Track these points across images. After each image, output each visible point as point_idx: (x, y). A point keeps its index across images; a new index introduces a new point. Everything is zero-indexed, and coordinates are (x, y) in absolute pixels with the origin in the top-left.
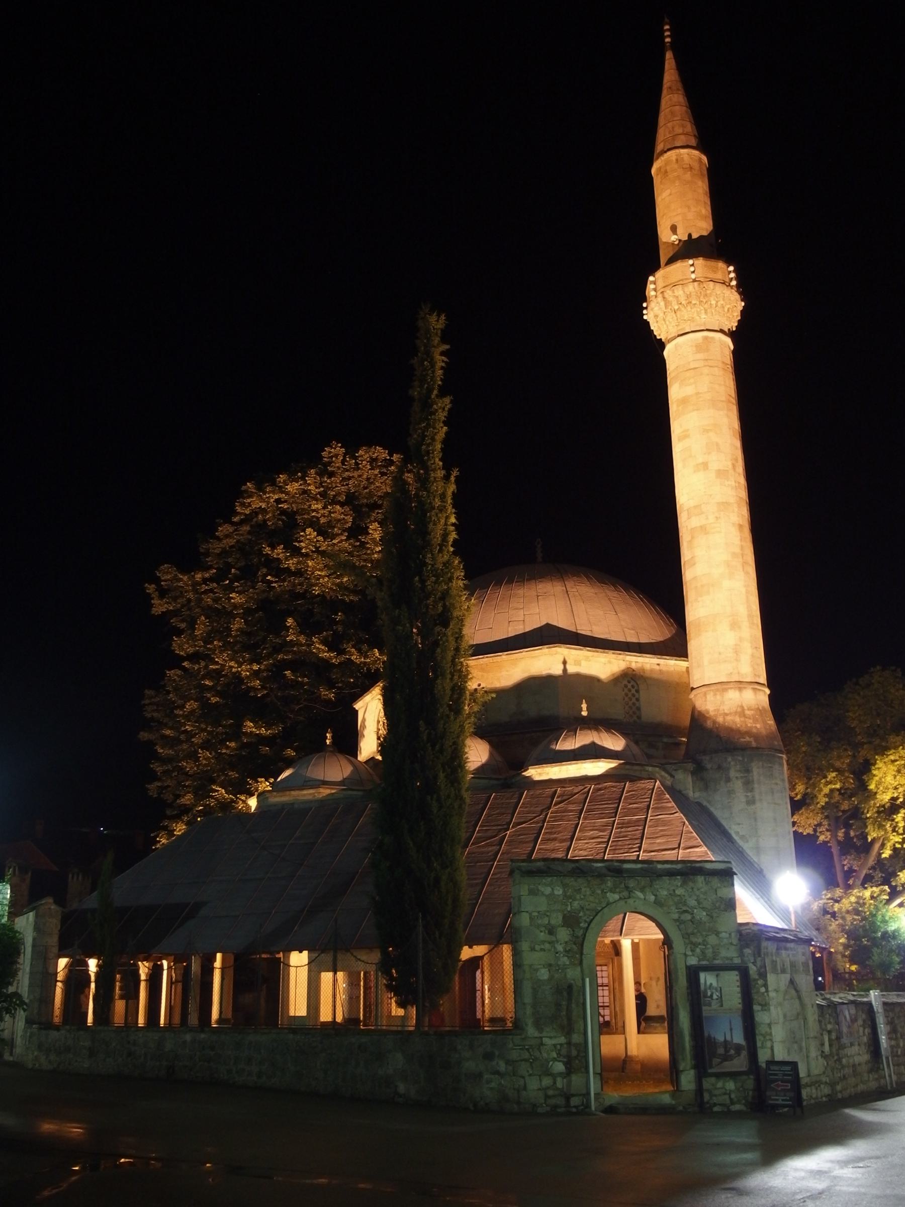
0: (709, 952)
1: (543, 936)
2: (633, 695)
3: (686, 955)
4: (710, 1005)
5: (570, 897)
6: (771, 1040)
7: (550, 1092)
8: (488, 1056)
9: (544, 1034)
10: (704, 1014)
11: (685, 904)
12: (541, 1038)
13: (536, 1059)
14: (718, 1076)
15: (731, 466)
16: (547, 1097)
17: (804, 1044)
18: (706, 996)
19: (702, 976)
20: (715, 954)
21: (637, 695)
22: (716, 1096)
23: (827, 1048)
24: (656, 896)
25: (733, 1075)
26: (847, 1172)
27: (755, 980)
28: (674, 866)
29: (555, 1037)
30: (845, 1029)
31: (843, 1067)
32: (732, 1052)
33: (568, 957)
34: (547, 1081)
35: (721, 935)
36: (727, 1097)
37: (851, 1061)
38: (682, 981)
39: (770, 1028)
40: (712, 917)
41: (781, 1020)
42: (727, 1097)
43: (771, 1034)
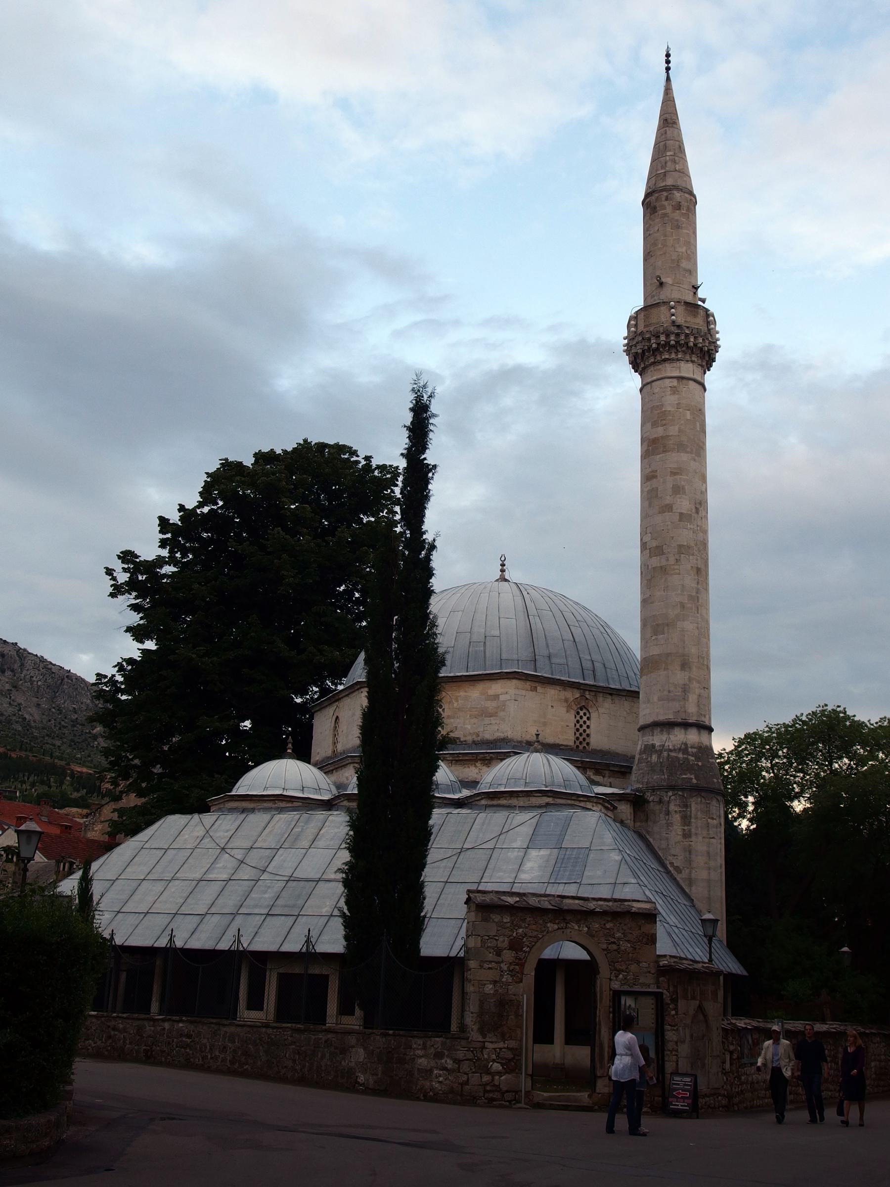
1: (491, 956)
3: (610, 979)
5: (516, 925)
7: (488, 1088)
8: (438, 1055)
9: (487, 1039)
11: (613, 936)
12: (484, 1042)
13: (479, 1059)
15: (694, 511)
16: (485, 1091)
21: (588, 723)
23: (727, 1066)
24: (589, 928)
27: (669, 1004)
29: (496, 1042)
30: (746, 1051)
33: (512, 976)
34: (486, 1078)
37: (750, 1079)
40: (635, 949)
41: (688, 1039)
43: (677, 1051)
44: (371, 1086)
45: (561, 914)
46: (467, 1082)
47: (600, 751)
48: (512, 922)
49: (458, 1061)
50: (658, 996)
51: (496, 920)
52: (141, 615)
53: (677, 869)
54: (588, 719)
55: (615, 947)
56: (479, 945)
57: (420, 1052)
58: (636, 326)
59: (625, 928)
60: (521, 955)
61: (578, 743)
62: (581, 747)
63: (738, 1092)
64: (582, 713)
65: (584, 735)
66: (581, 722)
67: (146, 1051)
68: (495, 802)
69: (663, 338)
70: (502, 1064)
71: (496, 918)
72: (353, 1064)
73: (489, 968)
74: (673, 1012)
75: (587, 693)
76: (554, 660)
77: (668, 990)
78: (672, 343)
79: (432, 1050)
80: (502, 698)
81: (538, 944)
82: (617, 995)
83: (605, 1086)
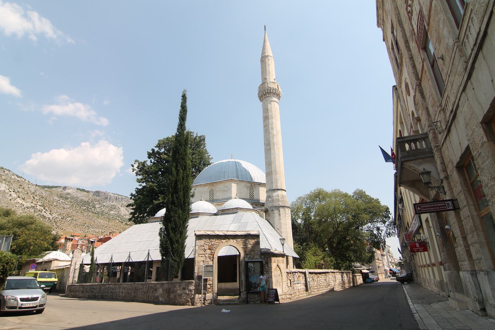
2: (252, 195)
4: (251, 272)
6: (269, 282)
8: (184, 289)
10: (249, 275)
14: (253, 293)
18: (250, 269)
19: (249, 264)
20: (253, 257)
22: (251, 299)
26: (368, 280)
30: (296, 279)
35: (255, 252)
36: (255, 299)
37: (298, 288)
39: (269, 279)
43: (269, 281)
44: (163, 302)
50: (261, 262)
52: (296, 256)
53: (278, 229)
54: (253, 191)
61: (250, 198)
62: (251, 199)
63: (294, 293)
64: (251, 190)
66: (251, 192)
67: (101, 295)
68: (224, 213)
72: (158, 295)
73: (201, 256)
80: (229, 187)
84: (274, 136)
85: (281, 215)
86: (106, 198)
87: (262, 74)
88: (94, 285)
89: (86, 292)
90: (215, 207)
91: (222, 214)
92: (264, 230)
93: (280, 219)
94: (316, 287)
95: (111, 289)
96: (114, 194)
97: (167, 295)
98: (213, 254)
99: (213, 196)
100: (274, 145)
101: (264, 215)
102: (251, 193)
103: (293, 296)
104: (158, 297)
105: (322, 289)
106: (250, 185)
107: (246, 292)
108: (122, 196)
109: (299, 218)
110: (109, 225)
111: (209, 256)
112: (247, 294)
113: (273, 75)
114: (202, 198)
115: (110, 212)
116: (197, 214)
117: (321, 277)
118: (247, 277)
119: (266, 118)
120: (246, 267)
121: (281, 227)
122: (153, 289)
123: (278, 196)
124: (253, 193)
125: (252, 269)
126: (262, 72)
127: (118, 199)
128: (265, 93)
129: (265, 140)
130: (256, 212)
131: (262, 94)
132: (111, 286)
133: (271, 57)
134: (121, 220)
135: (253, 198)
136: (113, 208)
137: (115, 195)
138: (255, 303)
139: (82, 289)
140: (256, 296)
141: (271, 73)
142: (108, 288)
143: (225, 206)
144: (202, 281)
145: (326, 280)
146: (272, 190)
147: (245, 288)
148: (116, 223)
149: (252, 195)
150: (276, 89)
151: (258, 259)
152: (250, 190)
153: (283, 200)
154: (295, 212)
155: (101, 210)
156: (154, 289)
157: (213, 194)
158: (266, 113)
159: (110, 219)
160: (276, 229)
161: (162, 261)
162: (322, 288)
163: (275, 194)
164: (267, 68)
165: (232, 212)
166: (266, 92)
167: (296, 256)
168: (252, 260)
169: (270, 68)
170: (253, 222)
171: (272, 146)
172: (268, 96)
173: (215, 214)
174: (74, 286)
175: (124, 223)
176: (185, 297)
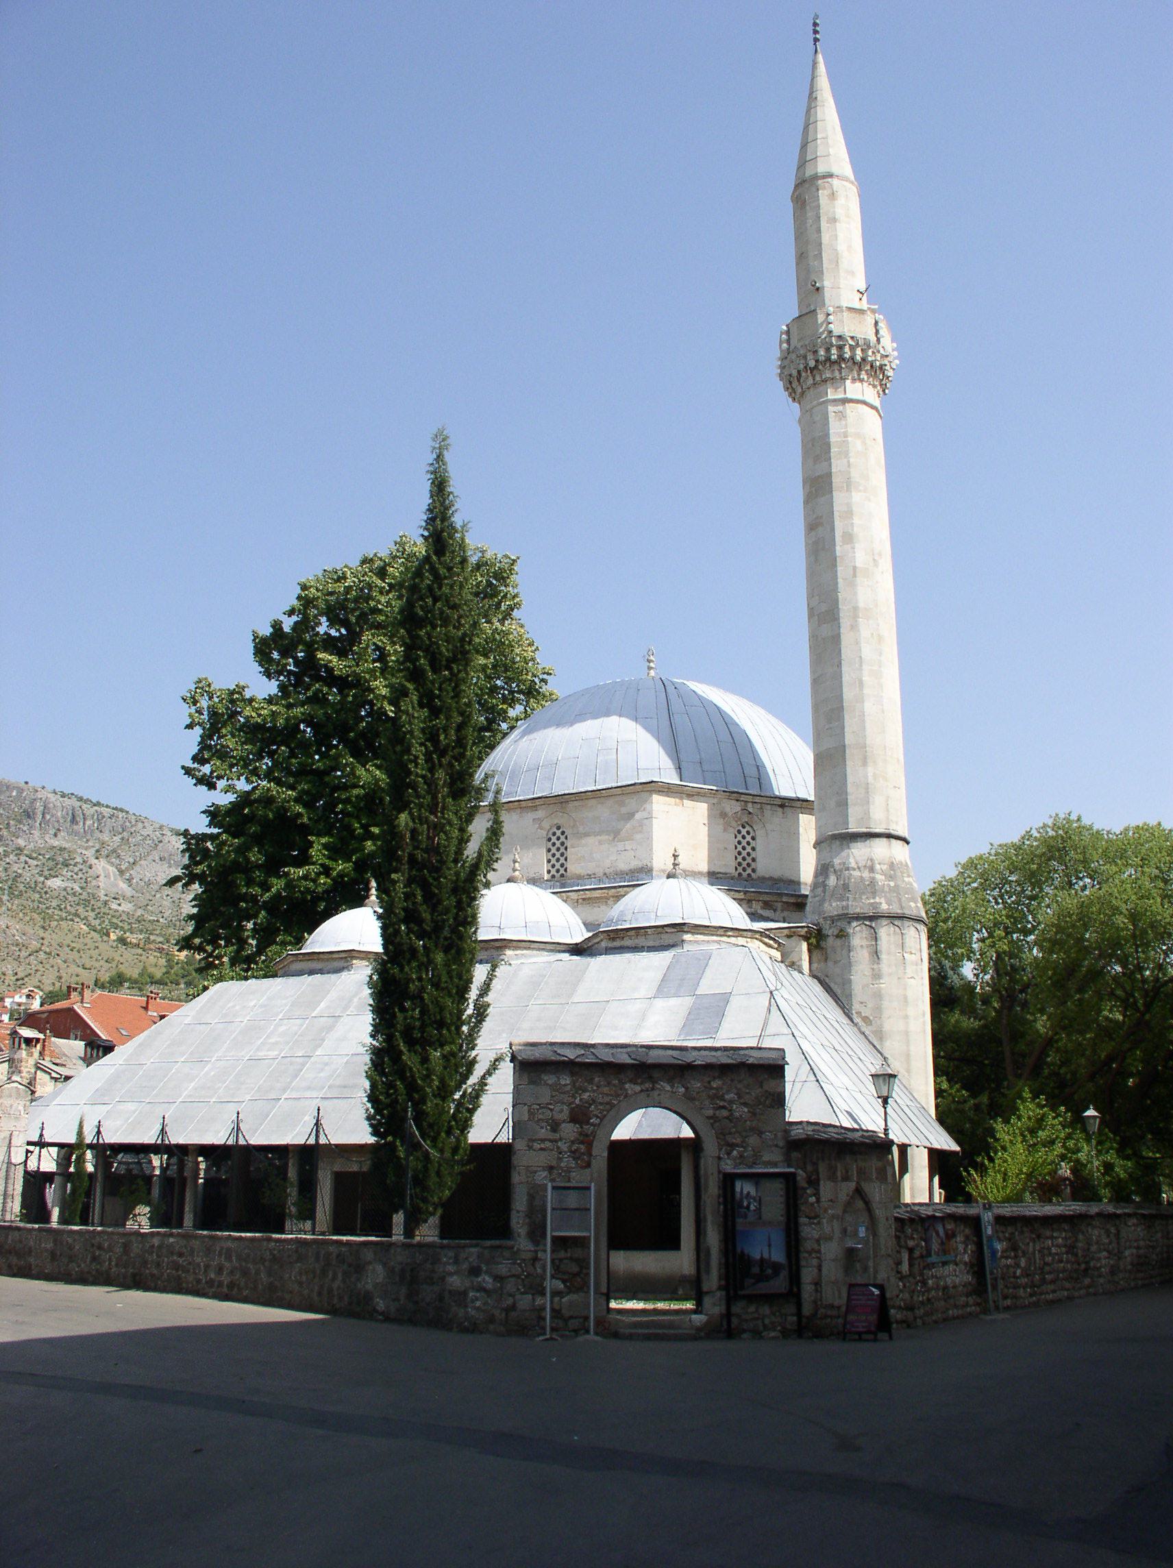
0: (748, 1153)
1: (544, 1133)
2: (748, 843)
3: (719, 1158)
4: (745, 1216)
8: (475, 1271)
10: (739, 1228)
12: (536, 1252)
14: (751, 1299)
17: (871, 1264)
18: (741, 1206)
21: (753, 843)
23: (905, 1268)
24: (687, 1089)
25: (768, 1298)
28: (713, 1053)
30: (935, 1246)
31: (929, 1290)
32: (770, 1271)
38: (712, 1189)
41: (837, 1234)
42: (759, 1322)
43: (819, 1251)
45: (646, 1073)
46: (514, 1307)
47: (771, 878)
48: (574, 1083)
49: (498, 1278)
50: (789, 1178)
51: (550, 1082)
52: (946, 1143)
53: (865, 1019)
55: (725, 1113)
56: (526, 1117)
57: (451, 1268)
58: (788, 342)
59: (739, 1086)
60: (588, 1129)
62: (745, 874)
63: (922, 1303)
64: (744, 832)
65: (749, 860)
66: (744, 843)
68: (617, 943)
69: (822, 352)
70: (564, 1281)
71: (550, 1079)
72: (369, 1287)
73: (542, 1149)
74: (813, 1199)
75: (750, 805)
76: (705, 767)
77: (804, 1169)
78: (834, 357)
79: (465, 1266)
81: (612, 1113)
82: (728, 1180)
83: (715, 1304)
84: (855, 575)
85: (883, 956)
86: (29, 815)
87: (797, 264)
88: (100, 1233)
89: (70, 1257)
90: (573, 908)
91: (608, 951)
92: (802, 1029)
93: (877, 976)
94: (1024, 1280)
95: (172, 1253)
96: (63, 796)
97: (404, 1291)
98: (587, 1140)
99: (562, 860)
100: (855, 617)
101: (805, 956)
102: (744, 848)
103: (920, 1312)
104: (368, 1297)
105: (1051, 1287)
106: (737, 807)
107: (724, 1293)
108: (98, 804)
109: (969, 959)
110: (46, 942)
111: (574, 1148)
112: (729, 1301)
113: (852, 273)
114: (514, 870)
115: (48, 883)
116: (497, 944)
117: (1052, 1238)
118: (730, 1236)
119: (819, 486)
120: (725, 1197)
121: (878, 1009)
122: (345, 1267)
123: (872, 869)
124: (753, 849)
125: (749, 1204)
126: (801, 257)
127: (80, 819)
128: (812, 364)
129: (810, 596)
130: (766, 944)
131: (802, 366)
132: (171, 1240)
133: (847, 180)
134: (98, 922)
135: (754, 871)
136: (58, 861)
137: (67, 802)
138: (757, 1334)
139: (50, 1246)
140: (766, 1310)
141: (844, 264)
142: (160, 1247)
143: (622, 913)
144: (545, 1245)
145: (1071, 1249)
146: (838, 839)
147: (720, 1279)
148: (75, 933)
149: (745, 858)
150: (868, 345)
151: (775, 1165)
152: (739, 832)
153: (892, 884)
154: (945, 942)
155: (6, 870)
156: (350, 1265)
157: (562, 850)
158: (817, 459)
159: (51, 917)
160: (857, 1020)
161: (378, 1155)
162: (1053, 1282)
163: (858, 853)
164: (825, 238)
165: (657, 944)
166: (822, 359)
167: (946, 1143)
168: (751, 1167)
169: (841, 236)
170: (750, 996)
171: (845, 622)
172: (828, 375)
173: (577, 950)
174: (16, 1233)
175: (113, 936)
176: (478, 1304)
